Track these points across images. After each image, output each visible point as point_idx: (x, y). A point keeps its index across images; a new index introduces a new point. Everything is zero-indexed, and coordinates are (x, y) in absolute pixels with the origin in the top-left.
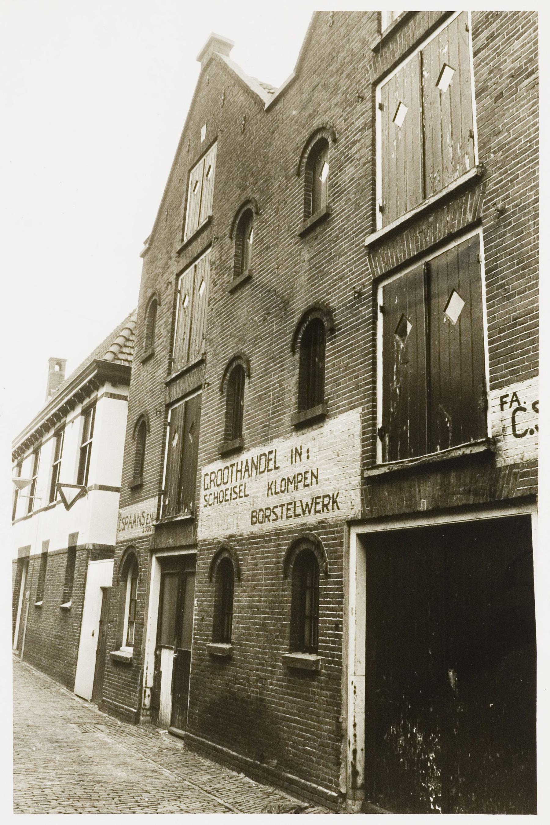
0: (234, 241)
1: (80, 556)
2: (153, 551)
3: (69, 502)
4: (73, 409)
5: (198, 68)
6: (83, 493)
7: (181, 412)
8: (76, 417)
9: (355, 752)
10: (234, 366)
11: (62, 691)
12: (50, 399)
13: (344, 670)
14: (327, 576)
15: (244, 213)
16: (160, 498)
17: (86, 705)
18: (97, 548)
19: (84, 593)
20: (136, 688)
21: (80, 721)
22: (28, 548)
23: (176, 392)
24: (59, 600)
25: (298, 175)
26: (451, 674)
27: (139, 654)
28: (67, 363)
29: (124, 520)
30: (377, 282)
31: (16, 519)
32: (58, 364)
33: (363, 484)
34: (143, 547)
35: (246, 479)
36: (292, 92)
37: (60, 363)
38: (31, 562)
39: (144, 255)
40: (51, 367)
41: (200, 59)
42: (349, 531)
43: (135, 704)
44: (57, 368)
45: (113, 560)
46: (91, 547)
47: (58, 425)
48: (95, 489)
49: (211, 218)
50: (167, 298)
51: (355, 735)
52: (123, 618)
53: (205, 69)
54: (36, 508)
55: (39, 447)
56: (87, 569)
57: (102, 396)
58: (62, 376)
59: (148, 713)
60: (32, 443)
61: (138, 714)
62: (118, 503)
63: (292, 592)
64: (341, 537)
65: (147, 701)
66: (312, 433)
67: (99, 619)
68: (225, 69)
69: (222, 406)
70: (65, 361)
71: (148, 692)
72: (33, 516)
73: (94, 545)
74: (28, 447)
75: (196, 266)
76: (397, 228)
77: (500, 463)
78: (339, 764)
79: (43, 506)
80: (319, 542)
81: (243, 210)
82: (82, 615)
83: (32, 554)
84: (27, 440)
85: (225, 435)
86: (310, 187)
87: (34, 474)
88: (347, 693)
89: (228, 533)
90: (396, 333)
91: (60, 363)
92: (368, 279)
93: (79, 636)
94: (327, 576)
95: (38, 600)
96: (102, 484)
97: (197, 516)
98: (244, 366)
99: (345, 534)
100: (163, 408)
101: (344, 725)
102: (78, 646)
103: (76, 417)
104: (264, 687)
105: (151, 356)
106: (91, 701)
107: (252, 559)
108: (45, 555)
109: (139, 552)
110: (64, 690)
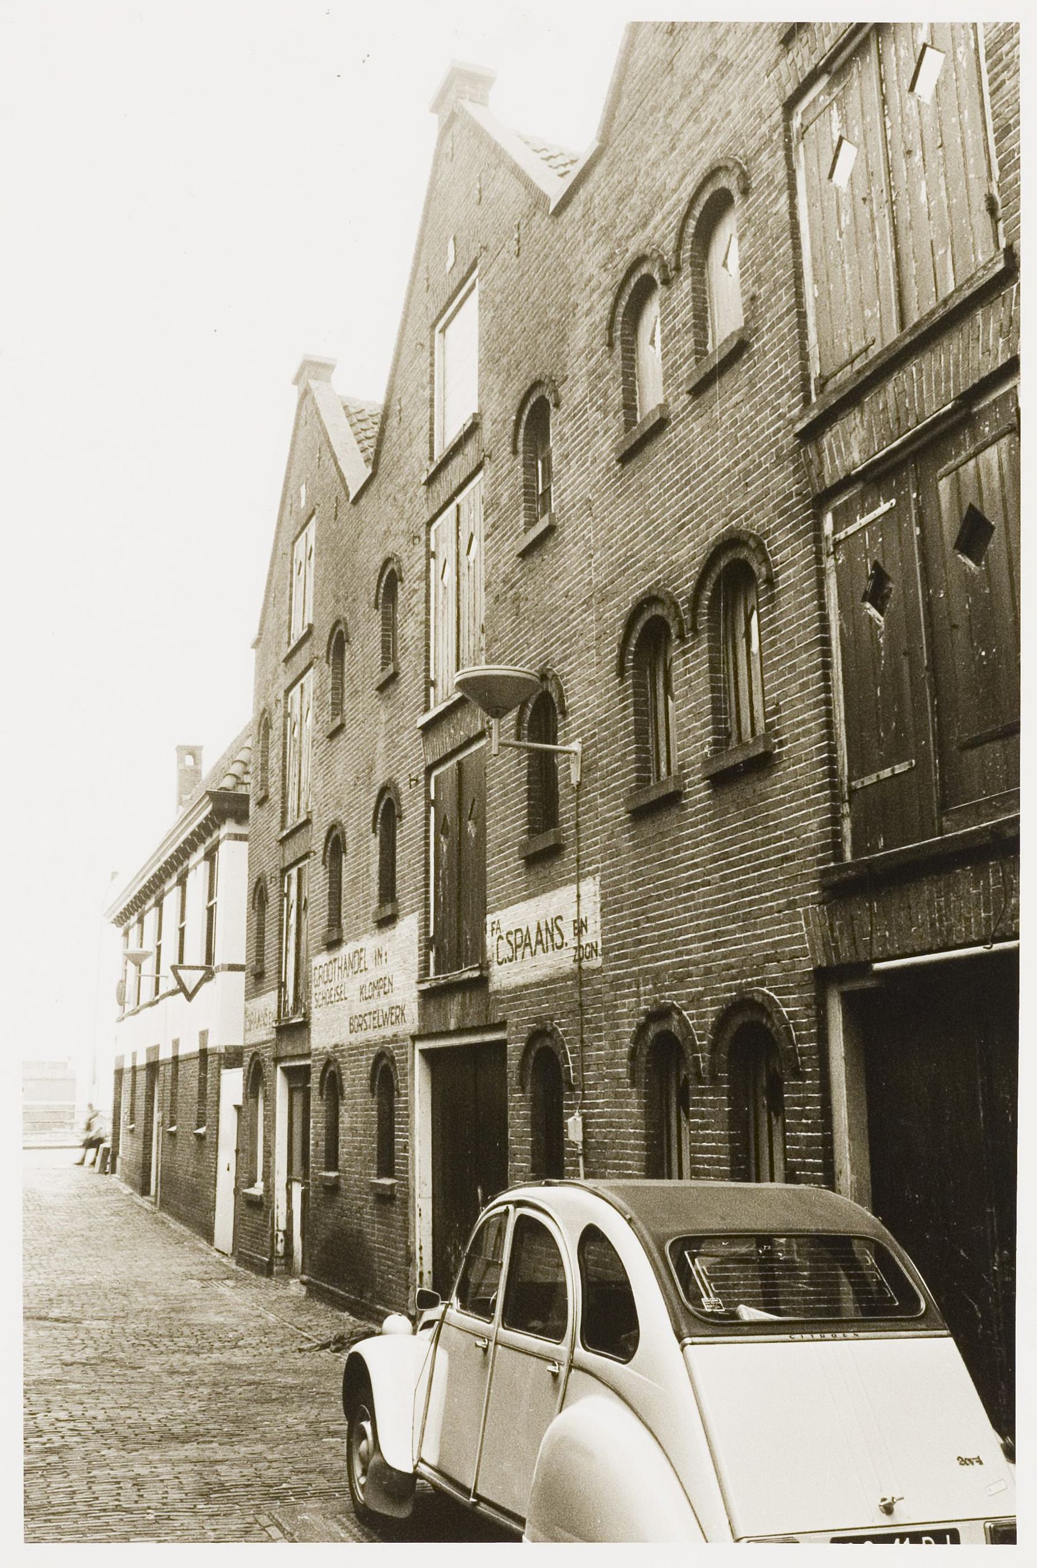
0: (521, 456)
1: (212, 1062)
2: (277, 1060)
3: (190, 990)
4: (195, 849)
5: (433, 124)
6: (209, 975)
7: (450, 783)
8: (198, 863)
9: (421, 1274)
10: (723, 563)
11: (201, 1245)
12: (183, 810)
13: (411, 1193)
14: (399, 1095)
15: (533, 406)
16: (280, 992)
17: (224, 1260)
18: (232, 1050)
19: (218, 1113)
20: (267, 1232)
21: (206, 1276)
22: (155, 1049)
23: (446, 740)
24: (194, 1123)
25: (376, 607)
26: (479, 1191)
27: (269, 1189)
28: (203, 751)
29: (511, 938)
30: (429, 770)
31: (141, 1003)
32: (190, 754)
33: (420, 997)
34: (268, 1053)
35: (345, 980)
36: (599, 170)
37: (193, 752)
38: (161, 1068)
39: (256, 644)
40: (181, 760)
41: (436, 108)
42: (413, 1046)
43: (266, 1252)
44: (189, 760)
45: (241, 1069)
46: (223, 1051)
47: (180, 869)
48: (223, 969)
49: (310, 626)
50: (277, 722)
51: (421, 1258)
52: (256, 1147)
53: (446, 128)
54: (162, 991)
55: (162, 898)
56: (219, 1081)
57: (224, 838)
58: (197, 773)
59: (283, 1261)
60: (153, 892)
61: (270, 1264)
62: (243, 994)
63: (532, 1111)
64: (406, 1053)
65: (280, 1247)
66: (389, 933)
67: (235, 1148)
68: (477, 132)
69: (625, 708)
70: (201, 748)
71: (281, 1236)
72: (161, 1002)
73: (226, 1048)
74: (169, 875)
75: (302, 686)
76: (437, 716)
77: (493, 987)
78: (408, 1288)
79: (170, 989)
80: (393, 1057)
81: (633, 282)
82: (217, 1143)
83: (161, 1058)
84: (193, 833)
85: (329, 920)
86: (388, 625)
87: (211, 897)
88: (414, 1216)
89: (333, 1042)
90: (864, 600)
91: (193, 752)
92: (421, 767)
93: (216, 1172)
94: (399, 1095)
95: (172, 1124)
96: (231, 963)
97: (310, 1018)
98: (554, 695)
99: (410, 1050)
100: (278, 873)
101: (412, 1248)
102: (215, 1185)
103: (198, 863)
104: (361, 1219)
105: (340, 729)
106: (232, 1254)
107: (352, 1073)
108: (176, 1059)
109: (263, 1060)
110: (203, 1244)
